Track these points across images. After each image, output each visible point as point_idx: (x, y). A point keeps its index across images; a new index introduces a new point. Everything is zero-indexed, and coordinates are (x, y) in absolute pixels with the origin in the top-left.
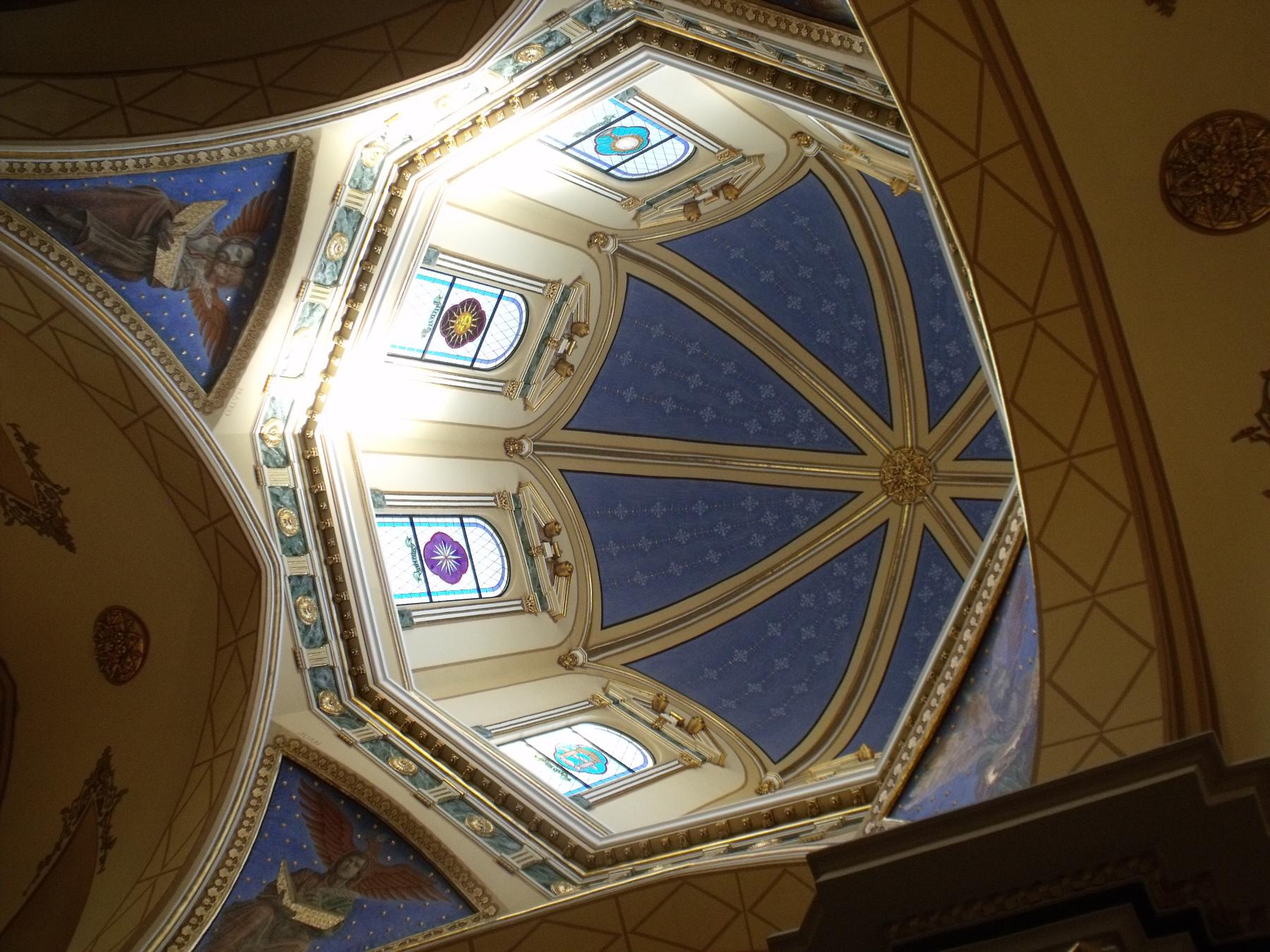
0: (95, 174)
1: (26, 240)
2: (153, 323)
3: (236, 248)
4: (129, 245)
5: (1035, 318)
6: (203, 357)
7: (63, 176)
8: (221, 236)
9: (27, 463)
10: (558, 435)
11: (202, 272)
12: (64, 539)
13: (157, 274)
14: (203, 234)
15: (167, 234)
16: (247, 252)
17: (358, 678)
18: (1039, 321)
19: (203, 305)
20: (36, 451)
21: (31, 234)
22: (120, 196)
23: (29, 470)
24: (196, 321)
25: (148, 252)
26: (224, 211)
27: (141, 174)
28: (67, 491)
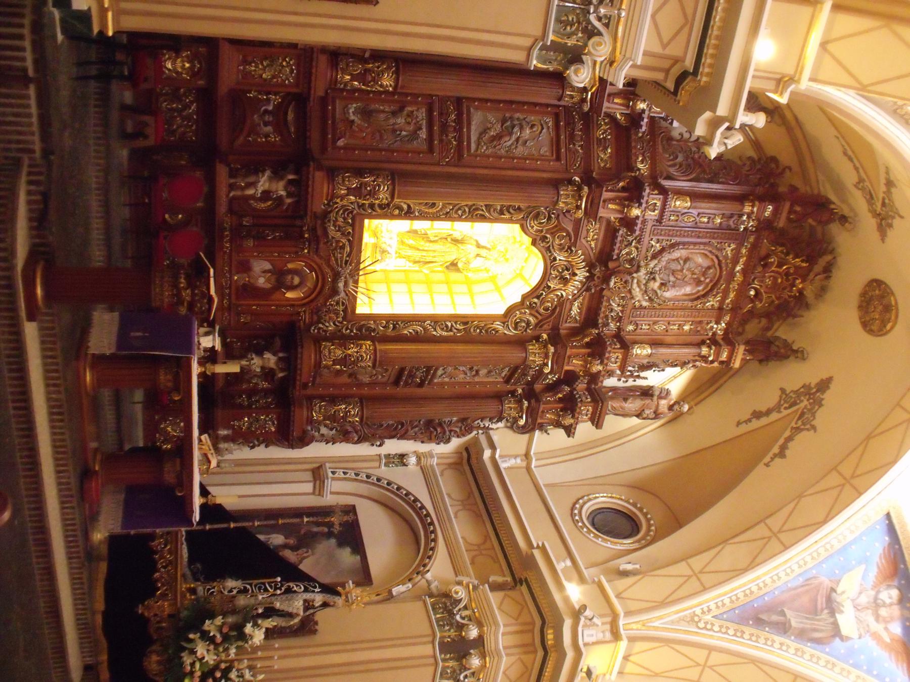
0: (779, 584)
1: (757, 641)
2: (856, 666)
4: (819, 620)
7: (762, 593)
15: (838, 603)
21: (758, 637)
25: (832, 620)
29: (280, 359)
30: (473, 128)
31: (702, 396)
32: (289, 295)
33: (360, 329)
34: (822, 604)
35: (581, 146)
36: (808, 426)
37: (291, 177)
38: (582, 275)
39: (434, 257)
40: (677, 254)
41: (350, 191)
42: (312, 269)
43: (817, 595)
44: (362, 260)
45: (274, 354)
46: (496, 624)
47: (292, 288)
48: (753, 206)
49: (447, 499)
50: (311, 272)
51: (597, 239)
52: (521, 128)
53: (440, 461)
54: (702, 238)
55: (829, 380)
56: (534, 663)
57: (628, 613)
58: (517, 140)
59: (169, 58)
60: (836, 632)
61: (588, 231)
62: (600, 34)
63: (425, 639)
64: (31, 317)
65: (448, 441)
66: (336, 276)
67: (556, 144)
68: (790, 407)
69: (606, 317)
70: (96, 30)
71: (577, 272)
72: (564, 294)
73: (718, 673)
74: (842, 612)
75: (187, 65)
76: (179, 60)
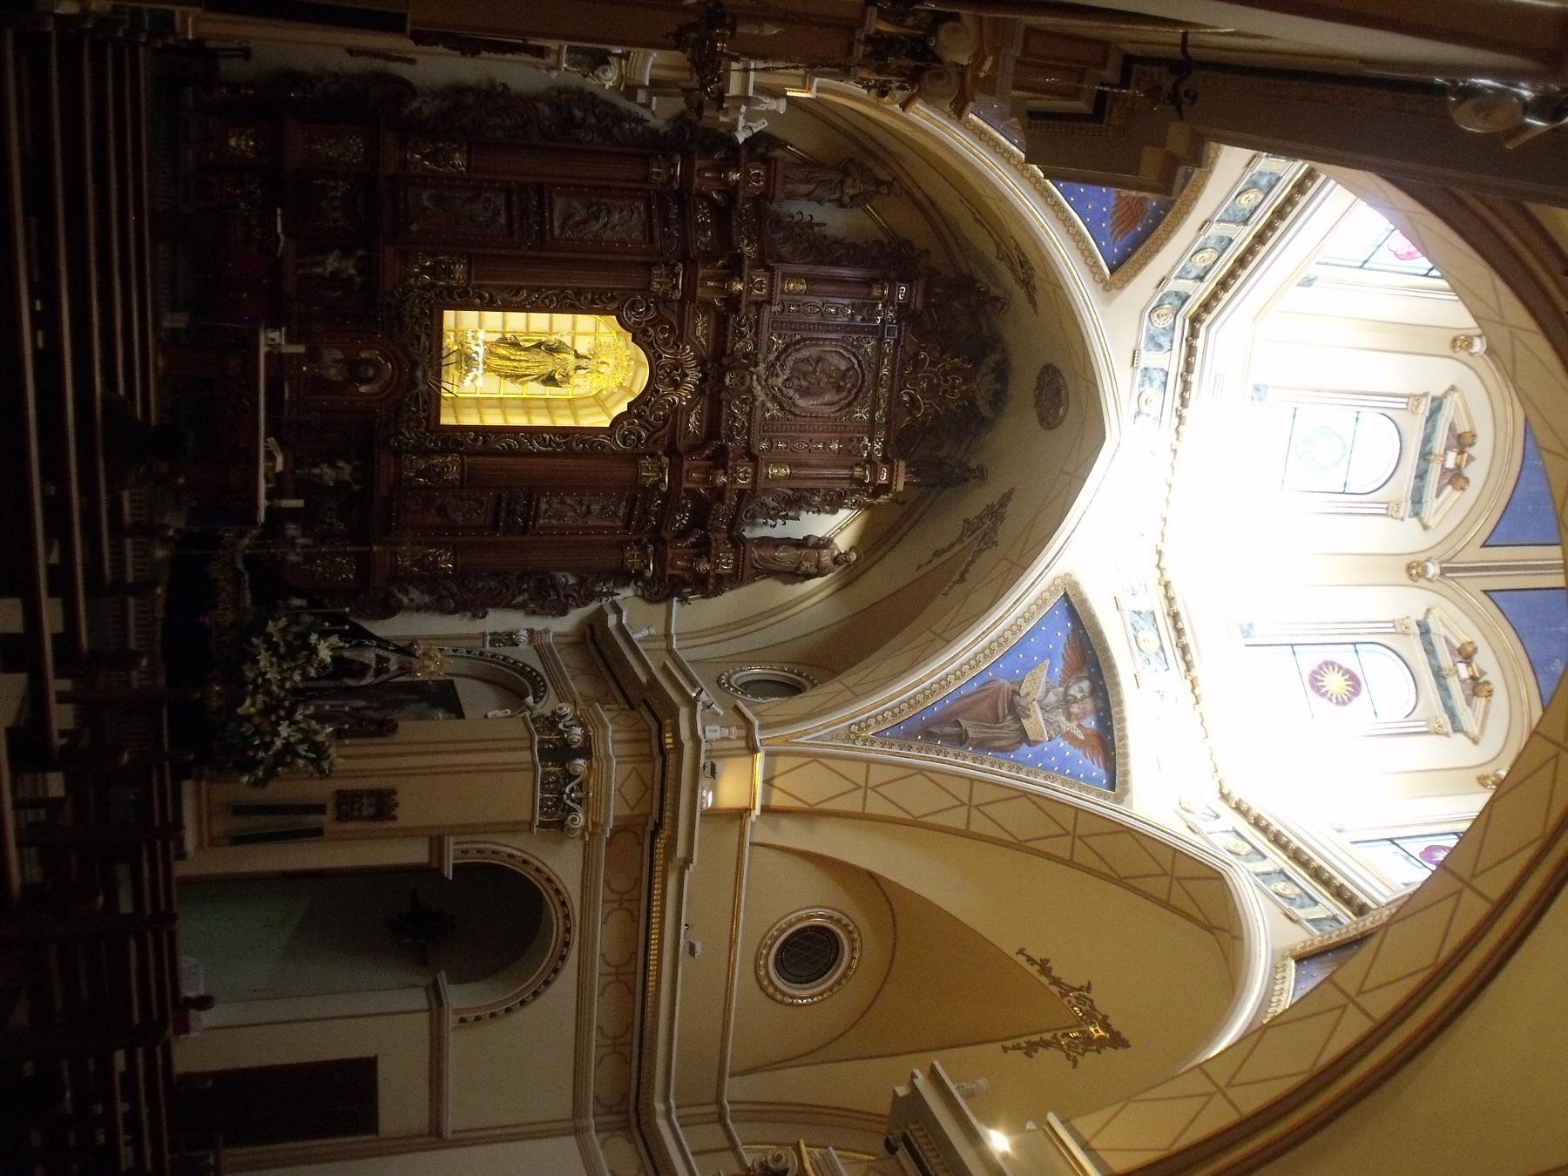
3: (1076, 687)
4: (1002, 728)
6: (1098, 771)
8: (1060, 686)
9: (1050, 984)
10: (1475, 555)
11: (1062, 719)
13: (1031, 737)
14: (1047, 692)
15: (1022, 707)
16: (1085, 685)
17: (1195, 320)
19: (1077, 739)
20: (1049, 965)
22: (975, 697)
23: (1055, 989)
24: (1079, 753)
25: (1017, 726)
26: (1051, 666)
27: (726, 329)
29: (356, 469)
30: (556, 216)
31: (880, 553)
32: (363, 389)
33: (445, 442)
34: (1003, 710)
35: (677, 229)
36: (990, 544)
37: (360, 253)
38: (693, 376)
39: (527, 368)
40: (805, 353)
41: (425, 270)
43: (997, 701)
44: (444, 355)
46: (605, 727)
47: (368, 381)
48: (883, 289)
49: (565, 669)
50: (386, 362)
51: (706, 335)
52: (609, 212)
53: (558, 639)
54: (831, 332)
55: (1012, 491)
56: (653, 777)
57: (763, 727)
58: (605, 225)
59: (234, 136)
60: (1023, 737)
61: (696, 326)
63: (520, 744)
65: (563, 612)
66: (414, 365)
67: (648, 227)
68: (973, 532)
69: (731, 428)
71: (688, 372)
72: (677, 400)
73: (882, 796)
74: (1028, 716)
75: (251, 143)
76: (244, 137)
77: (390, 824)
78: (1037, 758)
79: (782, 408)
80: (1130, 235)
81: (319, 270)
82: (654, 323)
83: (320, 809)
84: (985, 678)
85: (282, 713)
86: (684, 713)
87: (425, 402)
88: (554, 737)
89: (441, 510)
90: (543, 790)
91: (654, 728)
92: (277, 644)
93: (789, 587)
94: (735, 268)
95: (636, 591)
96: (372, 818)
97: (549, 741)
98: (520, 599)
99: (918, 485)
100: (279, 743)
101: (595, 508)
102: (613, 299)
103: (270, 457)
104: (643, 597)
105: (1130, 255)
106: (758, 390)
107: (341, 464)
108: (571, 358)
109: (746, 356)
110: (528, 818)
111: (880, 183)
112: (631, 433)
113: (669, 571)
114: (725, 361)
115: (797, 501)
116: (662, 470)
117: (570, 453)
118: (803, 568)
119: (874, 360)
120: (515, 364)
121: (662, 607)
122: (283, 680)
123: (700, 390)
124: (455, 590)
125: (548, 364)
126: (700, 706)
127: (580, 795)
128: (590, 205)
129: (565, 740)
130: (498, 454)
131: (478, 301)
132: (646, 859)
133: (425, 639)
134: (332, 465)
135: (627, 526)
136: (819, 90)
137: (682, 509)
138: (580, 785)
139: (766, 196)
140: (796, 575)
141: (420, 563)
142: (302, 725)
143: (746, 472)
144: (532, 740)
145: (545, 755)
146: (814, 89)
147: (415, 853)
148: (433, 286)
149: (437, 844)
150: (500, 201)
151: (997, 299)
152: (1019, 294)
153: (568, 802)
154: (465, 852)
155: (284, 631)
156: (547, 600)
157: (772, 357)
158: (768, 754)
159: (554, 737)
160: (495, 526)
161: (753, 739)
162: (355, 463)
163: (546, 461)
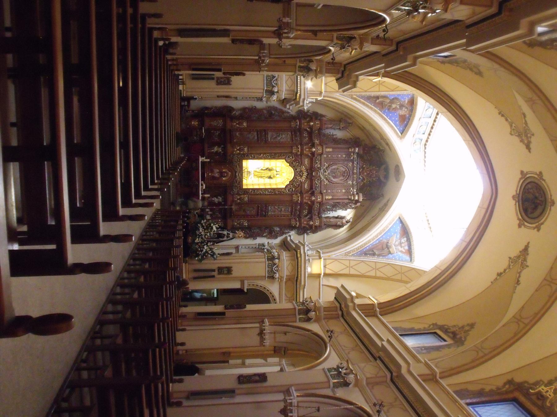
5: (350, 267)
6: (408, 258)
12: (526, 249)
14: (396, 242)
16: (405, 239)
18: (351, 266)
19: (403, 252)
24: (404, 255)
25: (388, 250)
26: (397, 236)
28: (510, 258)
33: (244, 192)
37: (222, 146)
38: (305, 174)
40: (334, 167)
41: (237, 150)
42: (229, 171)
45: (221, 197)
47: (225, 177)
48: (352, 149)
58: (281, 138)
60: (390, 253)
61: (305, 161)
62: (275, 86)
64: (181, 90)
65: (276, 238)
70: (182, 96)
71: (304, 173)
73: (354, 269)
77: (231, 276)
78: (393, 257)
79: (329, 181)
80: (404, 125)
81: (213, 151)
82: (295, 161)
83: (214, 271)
84: (379, 240)
85: (205, 243)
86: (302, 247)
87: (239, 183)
88: (270, 255)
89: (244, 211)
90: (268, 268)
91: (295, 253)
92: (204, 226)
93: (335, 230)
94: (313, 145)
95: (295, 232)
96: (226, 274)
97: (269, 256)
98: (265, 235)
99: (366, 200)
100: (204, 250)
101: (283, 209)
102: (284, 155)
103: (202, 185)
104: (297, 233)
105: (405, 129)
106: (322, 176)
107: (219, 197)
108: (275, 173)
109: (318, 168)
110: (264, 275)
111: (349, 123)
112: (290, 189)
113: (303, 225)
114: (313, 169)
115: (335, 206)
116: (298, 197)
117: (275, 194)
118: (338, 224)
119: (352, 168)
120: (261, 174)
121: (302, 236)
122: (205, 235)
123: (307, 177)
124: (248, 232)
125: (269, 173)
126: (306, 246)
127: (277, 269)
128: (277, 134)
129: (273, 256)
130: (257, 195)
131: (251, 157)
132: (295, 287)
133: (241, 245)
134: (217, 198)
135: (292, 214)
136: (324, 97)
137: (305, 209)
138: (277, 266)
139: (320, 129)
140: (337, 226)
141: (239, 224)
142: (210, 247)
143: (320, 197)
144: (265, 256)
145: (268, 259)
146: (322, 96)
147: (236, 285)
148: (239, 154)
149: (242, 283)
150: (255, 133)
151: (382, 150)
152: (387, 148)
153: (274, 271)
154: (249, 285)
155: (205, 223)
156: (272, 235)
157: (325, 168)
158: (324, 259)
159: (270, 255)
160: (258, 215)
161: (321, 256)
162: (223, 197)
163: (268, 196)
